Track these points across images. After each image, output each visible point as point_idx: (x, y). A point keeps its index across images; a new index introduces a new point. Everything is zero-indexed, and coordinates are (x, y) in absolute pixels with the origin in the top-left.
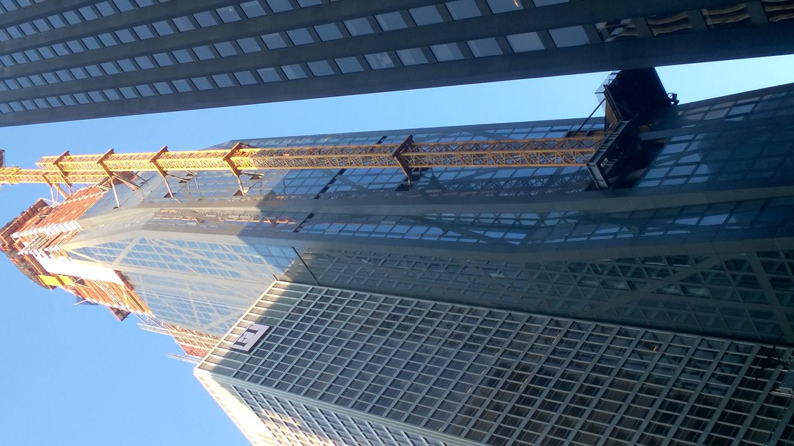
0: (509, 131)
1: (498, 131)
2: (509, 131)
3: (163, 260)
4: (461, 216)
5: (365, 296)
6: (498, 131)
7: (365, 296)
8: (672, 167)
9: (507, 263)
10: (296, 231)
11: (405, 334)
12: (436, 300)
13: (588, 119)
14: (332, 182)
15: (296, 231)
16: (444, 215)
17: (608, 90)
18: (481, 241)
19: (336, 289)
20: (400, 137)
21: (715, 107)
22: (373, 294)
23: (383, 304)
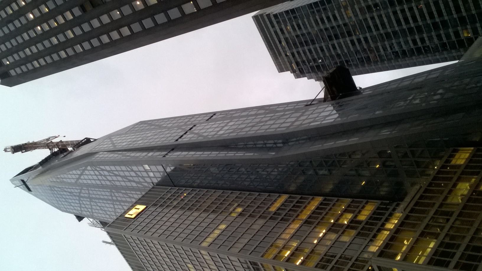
0: (276, 107)
1: (271, 108)
2: (276, 107)
3: (244, 196)
4: (248, 144)
5: (333, 200)
6: (271, 108)
7: (333, 200)
8: (318, 117)
9: (269, 165)
10: (164, 156)
11: (315, 221)
12: (186, 187)
13: (314, 100)
14: (185, 134)
15: (164, 156)
16: (239, 144)
17: (325, 79)
18: (255, 154)
19: (333, 198)
20: (208, 115)
21: (201, 116)
22: (327, 198)
23: (300, 200)
